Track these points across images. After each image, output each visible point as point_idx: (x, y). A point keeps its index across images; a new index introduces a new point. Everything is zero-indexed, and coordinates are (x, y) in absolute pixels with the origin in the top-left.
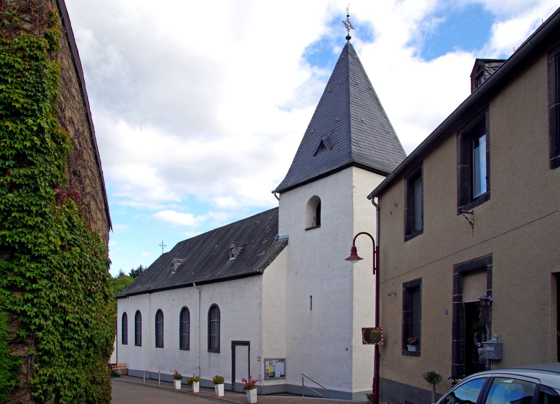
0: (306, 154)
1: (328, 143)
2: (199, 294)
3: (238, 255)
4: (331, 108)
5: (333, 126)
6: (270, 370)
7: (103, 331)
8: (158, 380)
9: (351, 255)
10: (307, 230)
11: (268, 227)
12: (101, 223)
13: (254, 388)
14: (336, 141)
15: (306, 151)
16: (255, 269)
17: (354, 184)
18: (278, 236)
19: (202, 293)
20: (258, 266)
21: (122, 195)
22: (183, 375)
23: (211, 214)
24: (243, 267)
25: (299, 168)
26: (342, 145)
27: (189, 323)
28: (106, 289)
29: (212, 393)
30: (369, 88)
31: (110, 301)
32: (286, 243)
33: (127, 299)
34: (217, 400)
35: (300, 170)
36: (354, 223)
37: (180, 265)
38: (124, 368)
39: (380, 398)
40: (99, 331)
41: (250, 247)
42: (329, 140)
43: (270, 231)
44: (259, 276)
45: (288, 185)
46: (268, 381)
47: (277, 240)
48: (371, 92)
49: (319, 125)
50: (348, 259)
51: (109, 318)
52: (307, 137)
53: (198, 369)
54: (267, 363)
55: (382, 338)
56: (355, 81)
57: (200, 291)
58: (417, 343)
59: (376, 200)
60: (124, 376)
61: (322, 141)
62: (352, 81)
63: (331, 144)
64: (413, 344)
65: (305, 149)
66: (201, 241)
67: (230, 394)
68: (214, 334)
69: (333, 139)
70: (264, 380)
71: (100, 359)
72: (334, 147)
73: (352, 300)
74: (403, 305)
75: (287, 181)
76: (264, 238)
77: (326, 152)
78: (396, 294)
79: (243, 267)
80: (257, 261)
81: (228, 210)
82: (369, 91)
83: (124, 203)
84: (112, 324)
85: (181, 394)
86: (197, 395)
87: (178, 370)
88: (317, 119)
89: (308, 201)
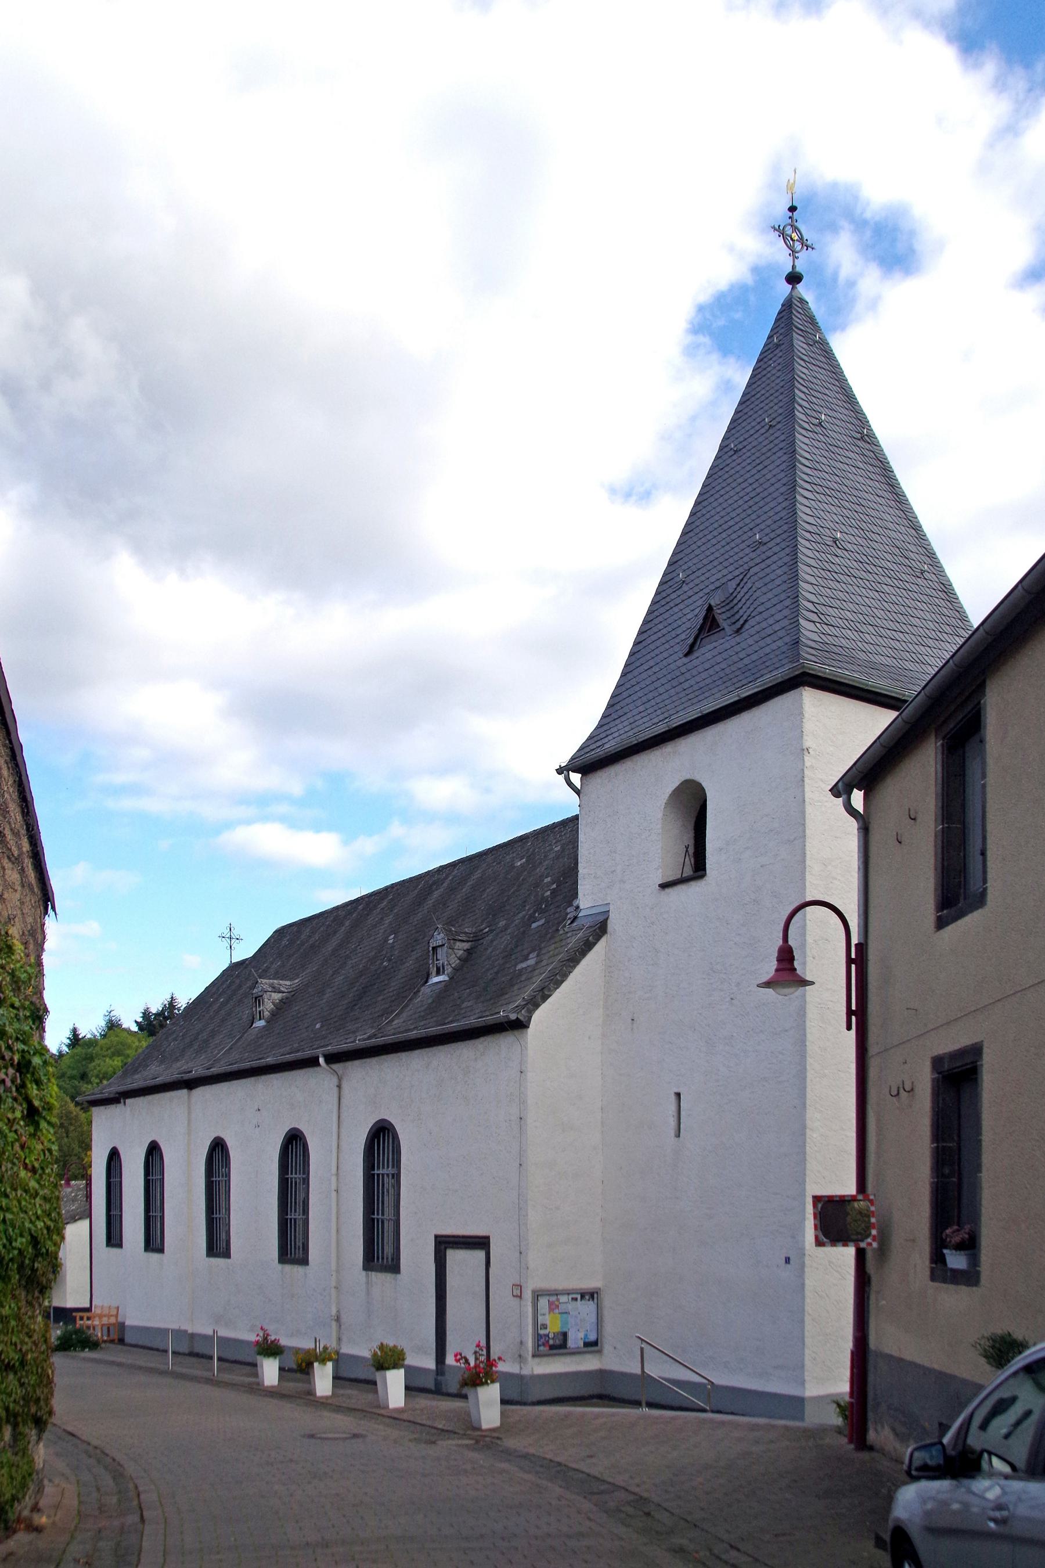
0: (662, 649)
1: (728, 614)
2: (336, 1089)
3: (454, 969)
4: (740, 502)
5: (746, 559)
6: (553, 1325)
7: (22, 1215)
8: (211, 1358)
9: (777, 970)
10: (664, 886)
11: (549, 879)
12: (18, 896)
13: (493, 1382)
14: (752, 609)
15: (663, 640)
16: (506, 1012)
17: (808, 742)
18: (578, 907)
19: (345, 1085)
20: (516, 1001)
21: (120, 778)
22: (284, 1342)
23: (396, 829)
24: (469, 1004)
25: (640, 694)
26: (771, 621)
27: (306, 1181)
28: (33, 1090)
29: (370, 1397)
30: (859, 436)
31: (46, 1125)
32: (601, 928)
33: (120, 1107)
34: (380, 1418)
35: (644, 699)
36: (808, 863)
37: (281, 1001)
38: (113, 1320)
39: (870, 1415)
40: (9, 1216)
41: (492, 941)
42: (731, 605)
43: (553, 891)
44: (516, 1032)
45: (607, 746)
46: (545, 1359)
47: (575, 918)
48: (867, 446)
49: (701, 557)
50: (768, 984)
51: (41, 1175)
52: (664, 594)
53: (334, 1324)
54: (543, 1303)
55: (873, 1226)
56: (815, 414)
57: (340, 1080)
58: (970, 1245)
59: (857, 798)
60: (111, 1346)
61: (710, 609)
62: (806, 414)
63: (737, 617)
64: (960, 1247)
65: (660, 634)
66: (347, 923)
67: (424, 1402)
68: (383, 1214)
69: (743, 600)
70: (534, 1356)
71: (14, 1297)
72: (747, 626)
73: (804, 1105)
74: (932, 1126)
75: (604, 735)
76: (535, 912)
77: (722, 641)
78: (912, 1090)
79: (469, 1004)
80: (513, 985)
81: (452, 818)
82: (859, 443)
83: (128, 804)
84: (53, 1192)
85: (275, 1401)
86: (323, 1404)
87: (271, 1328)
88: (695, 539)
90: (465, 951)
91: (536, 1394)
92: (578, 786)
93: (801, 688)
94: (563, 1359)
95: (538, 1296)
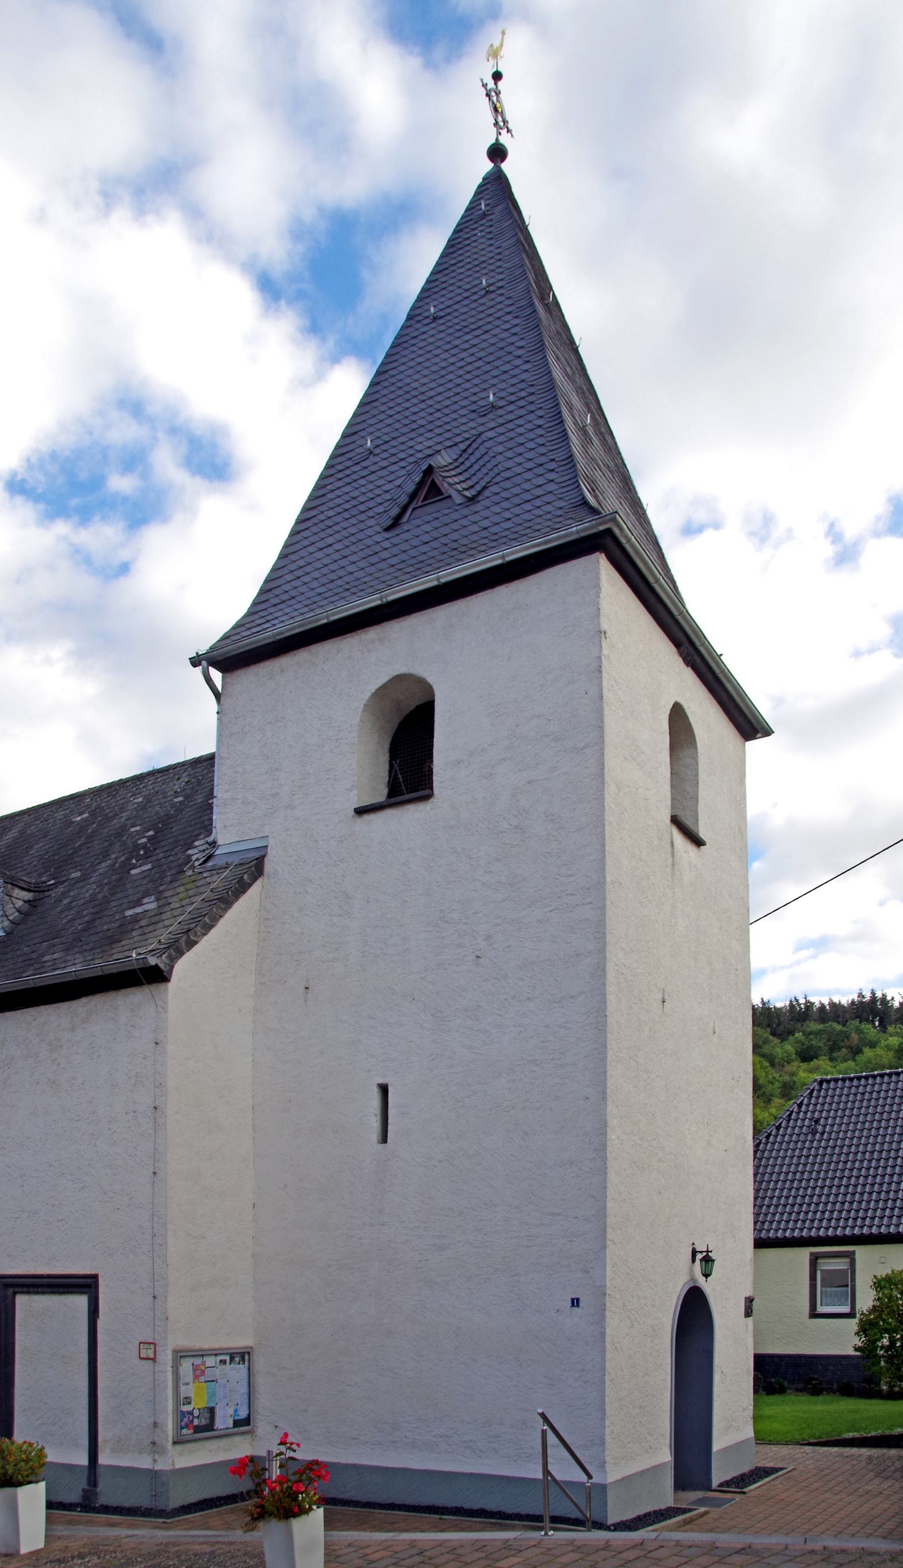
10: (361, 811)
54: (186, 1366)
70: (175, 1443)
72: (487, 493)
73: (604, 1096)
89: (367, 694)
90: (25, 902)
91: (177, 1499)
92: (219, 687)
93: (598, 553)
94: (209, 1444)
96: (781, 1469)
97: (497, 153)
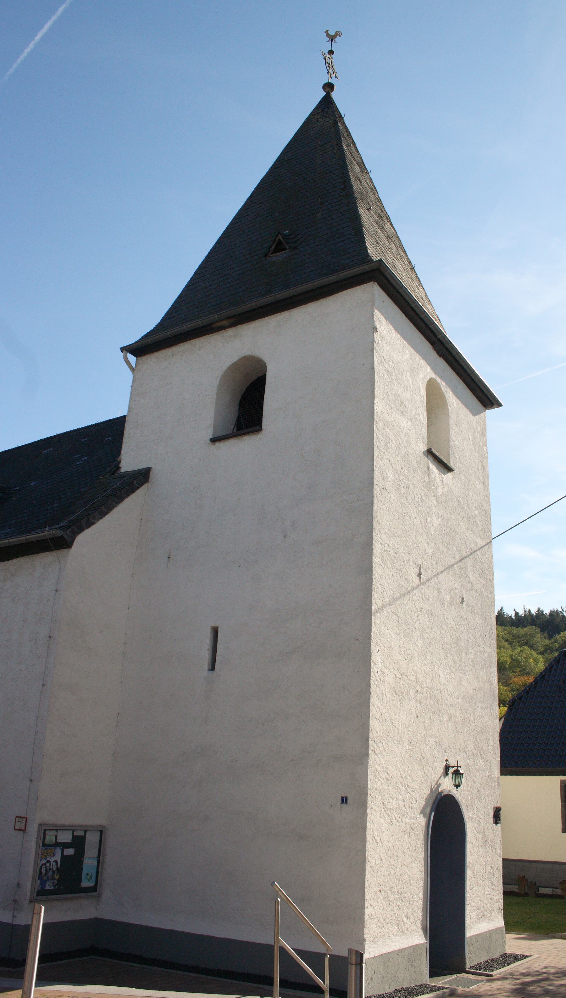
44: (59, 552)
92: (134, 365)
95: (45, 831)
96: (528, 956)
97: (329, 87)
